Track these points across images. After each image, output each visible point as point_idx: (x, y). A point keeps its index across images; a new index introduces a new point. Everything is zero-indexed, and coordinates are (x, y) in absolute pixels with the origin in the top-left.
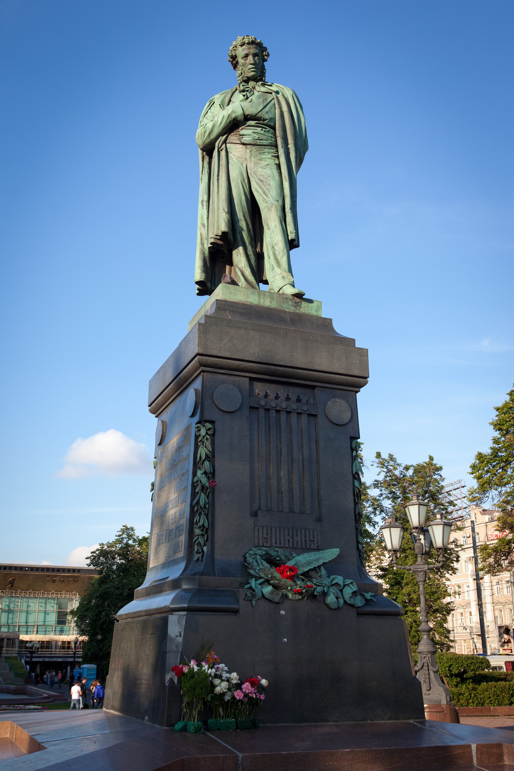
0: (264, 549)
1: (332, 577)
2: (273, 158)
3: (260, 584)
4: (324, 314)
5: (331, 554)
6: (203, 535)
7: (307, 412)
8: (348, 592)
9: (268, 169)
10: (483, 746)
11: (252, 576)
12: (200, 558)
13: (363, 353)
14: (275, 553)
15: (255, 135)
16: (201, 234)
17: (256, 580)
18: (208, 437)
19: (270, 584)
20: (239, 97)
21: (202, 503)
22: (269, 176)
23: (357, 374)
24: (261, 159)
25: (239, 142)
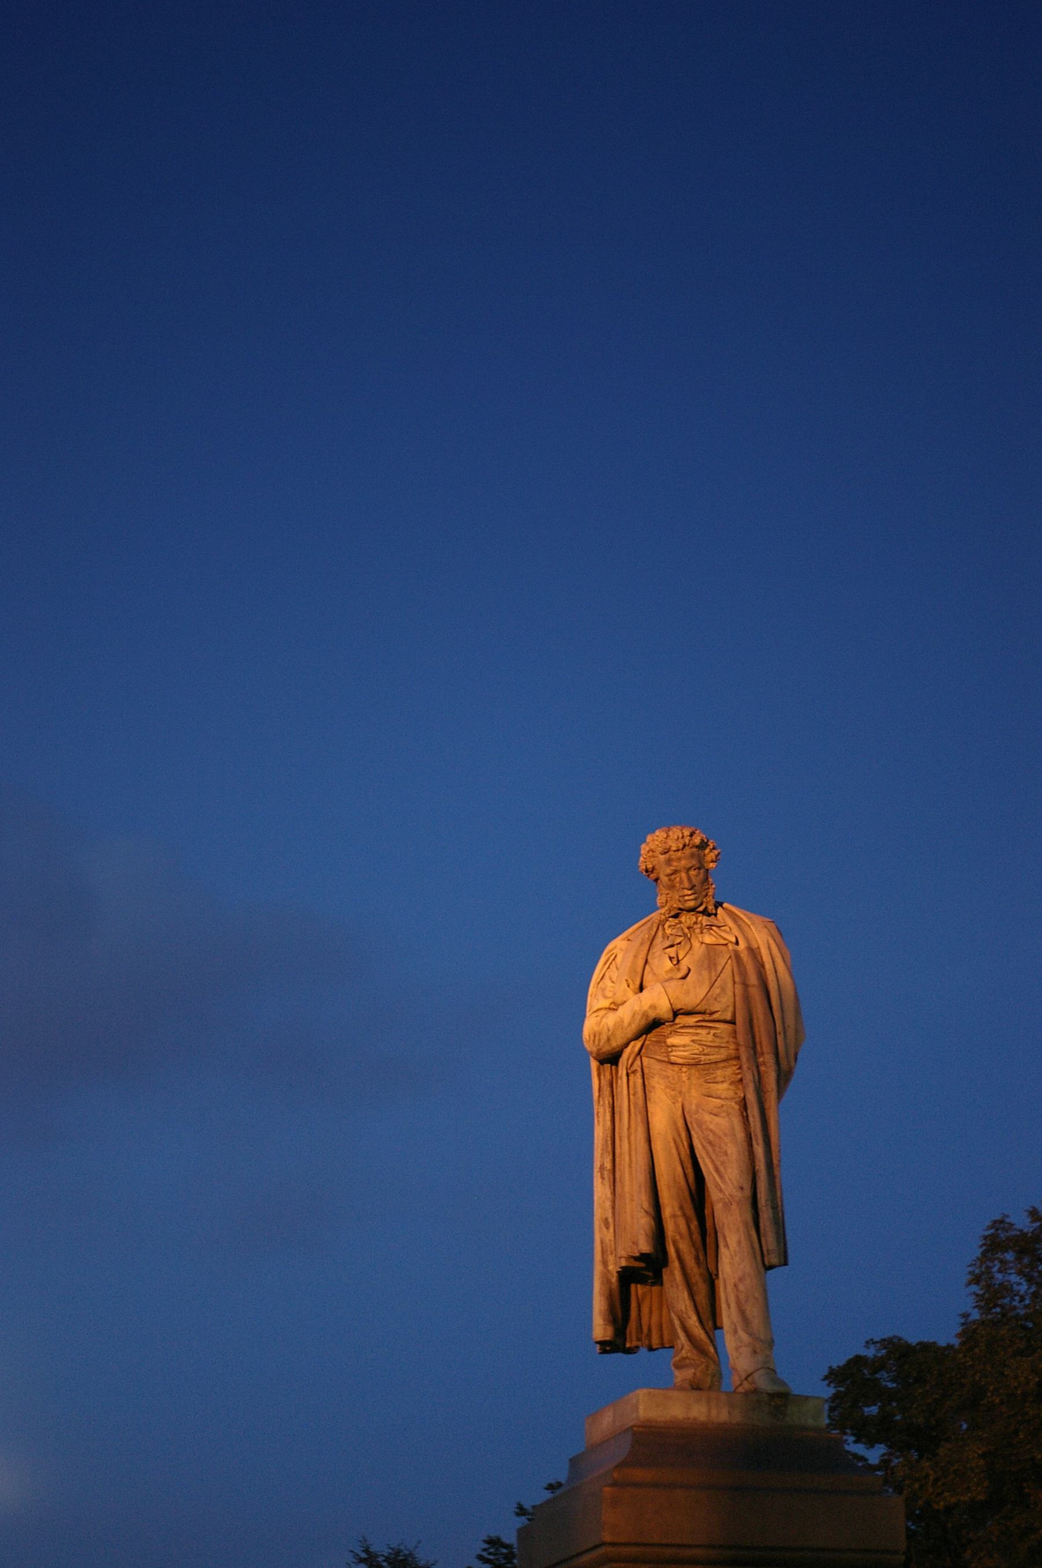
9: (723, 1115)
16: (602, 1242)
22: (725, 1135)
25: (666, 1059)
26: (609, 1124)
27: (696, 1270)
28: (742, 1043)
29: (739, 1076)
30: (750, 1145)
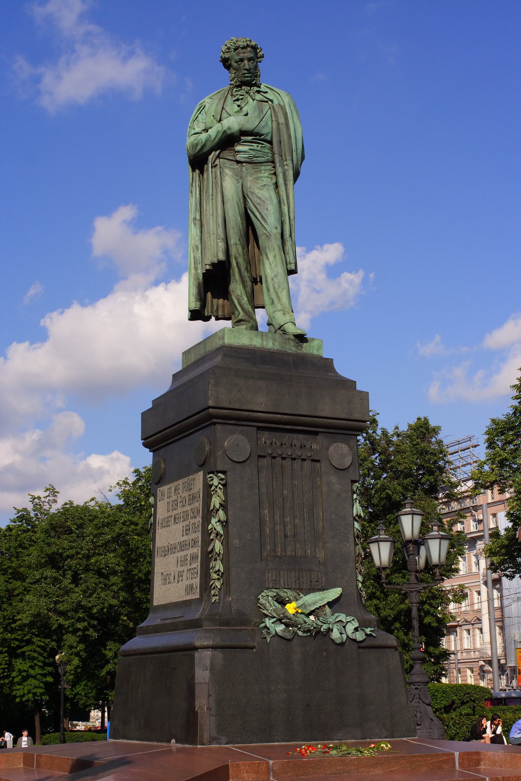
0: (274, 590)
1: (336, 614)
2: (270, 176)
3: (273, 623)
4: (325, 354)
5: (334, 593)
6: (218, 579)
7: (311, 458)
8: (350, 628)
9: (265, 190)
10: (465, 754)
11: (266, 616)
12: (217, 600)
13: (364, 396)
14: (285, 594)
15: (251, 152)
17: (269, 620)
18: (220, 486)
19: (282, 623)
20: (231, 107)
21: (217, 550)
23: (358, 419)
24: (257, 178)
25: (234, 159)
26: (198, 196)
27: (246, 274)
28: (276, 152)
29: (273, 172)
30: (280, 207)
